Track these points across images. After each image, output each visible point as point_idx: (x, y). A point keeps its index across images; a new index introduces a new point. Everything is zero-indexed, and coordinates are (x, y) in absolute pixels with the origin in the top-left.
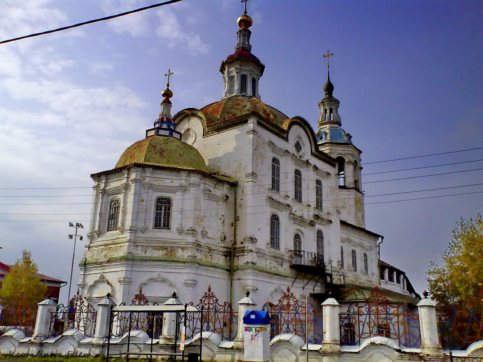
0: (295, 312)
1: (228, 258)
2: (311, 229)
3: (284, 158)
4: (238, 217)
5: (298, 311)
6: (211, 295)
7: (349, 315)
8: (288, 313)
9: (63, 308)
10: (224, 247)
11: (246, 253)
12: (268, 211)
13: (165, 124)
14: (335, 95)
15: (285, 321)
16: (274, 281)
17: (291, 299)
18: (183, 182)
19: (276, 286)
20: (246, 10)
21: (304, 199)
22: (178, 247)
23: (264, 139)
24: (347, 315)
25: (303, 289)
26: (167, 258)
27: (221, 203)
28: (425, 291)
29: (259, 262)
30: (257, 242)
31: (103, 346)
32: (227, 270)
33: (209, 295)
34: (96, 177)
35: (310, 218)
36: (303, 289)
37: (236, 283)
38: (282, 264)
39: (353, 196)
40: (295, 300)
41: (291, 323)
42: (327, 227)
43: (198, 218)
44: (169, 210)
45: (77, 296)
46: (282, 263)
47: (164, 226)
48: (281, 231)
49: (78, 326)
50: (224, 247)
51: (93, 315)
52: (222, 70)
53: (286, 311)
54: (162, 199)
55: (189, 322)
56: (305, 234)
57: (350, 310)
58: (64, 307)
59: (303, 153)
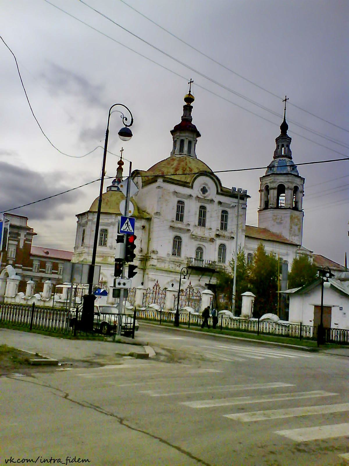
1: (143, 262)
2: (211, 244)
3: (188, 200)
4: (150, 238)
10: (141, 256)
11: (150, 260)
12: (172, 235)
13: (116, 183)
14: (288, 133)
16: (171, 276)
18: (113, 220)
19: (173, 279)
20: (190, 90)
21: (207, 224)
22: (109, 256)
23: (169, 190)
25: (199, 281)
26: (103, 262)
27: (140, 230)
29: (159, 264)
30: (159, 253)
31: (64, 303)
32: (142, 269)
34: (78, 216)
35: (210, 236)
36: (199, 281)
37: (146, 276)
38: (180, 266)
39: (289, 215)
42: (230, 242)
44: (107, 235)
46: (179, 265)
47: (104, 244)
48: (183, 246)
49: (191, 305)
50: (141, 256)
54: (103, 230)
56: (206, 247)
59: (208, 194)
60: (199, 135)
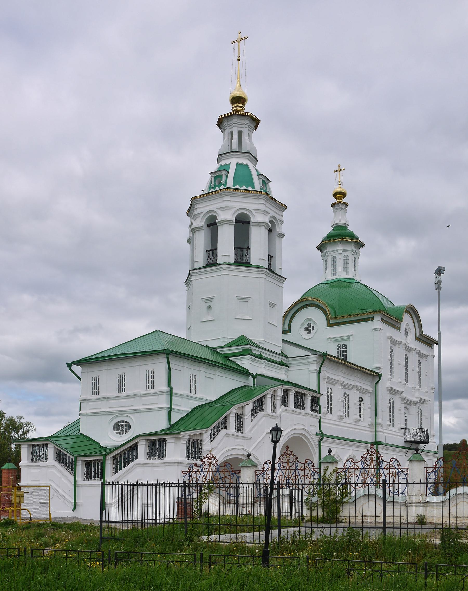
0: (294, 468)
5: (297, 467)
6: (290, 453)
7: (189, 472)
8: (288, 470)
9: (353, 464)
15: (285, 476)
17: (291, 456)
24: (261, 471)
28: (330, 449)
33: (288, 453)
40: (294, 457)
41: (291, 478)
43: (21, 417)
45: (287, 452)
47: (315, 398)
51: (313, 471)
52: (321, 248)
53: (369, 466)
55: (267, 480)
57: (346, 465)
58: (354, 463)
60: (361, 245)
